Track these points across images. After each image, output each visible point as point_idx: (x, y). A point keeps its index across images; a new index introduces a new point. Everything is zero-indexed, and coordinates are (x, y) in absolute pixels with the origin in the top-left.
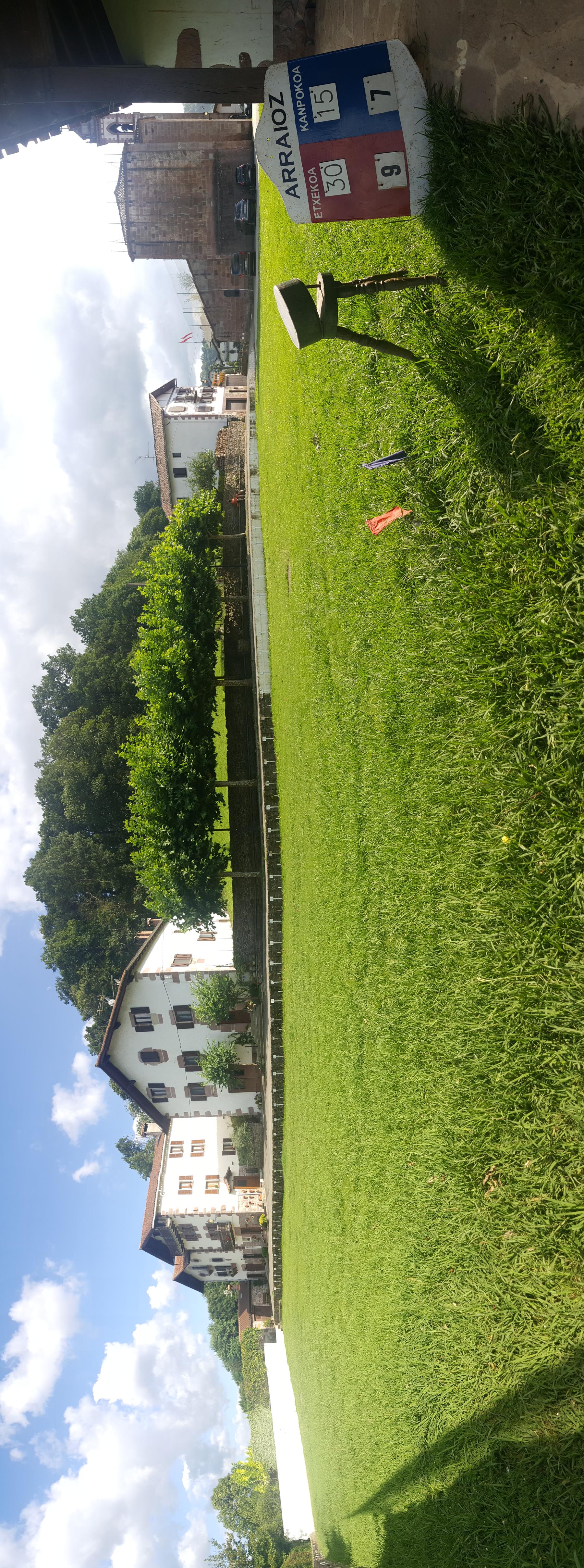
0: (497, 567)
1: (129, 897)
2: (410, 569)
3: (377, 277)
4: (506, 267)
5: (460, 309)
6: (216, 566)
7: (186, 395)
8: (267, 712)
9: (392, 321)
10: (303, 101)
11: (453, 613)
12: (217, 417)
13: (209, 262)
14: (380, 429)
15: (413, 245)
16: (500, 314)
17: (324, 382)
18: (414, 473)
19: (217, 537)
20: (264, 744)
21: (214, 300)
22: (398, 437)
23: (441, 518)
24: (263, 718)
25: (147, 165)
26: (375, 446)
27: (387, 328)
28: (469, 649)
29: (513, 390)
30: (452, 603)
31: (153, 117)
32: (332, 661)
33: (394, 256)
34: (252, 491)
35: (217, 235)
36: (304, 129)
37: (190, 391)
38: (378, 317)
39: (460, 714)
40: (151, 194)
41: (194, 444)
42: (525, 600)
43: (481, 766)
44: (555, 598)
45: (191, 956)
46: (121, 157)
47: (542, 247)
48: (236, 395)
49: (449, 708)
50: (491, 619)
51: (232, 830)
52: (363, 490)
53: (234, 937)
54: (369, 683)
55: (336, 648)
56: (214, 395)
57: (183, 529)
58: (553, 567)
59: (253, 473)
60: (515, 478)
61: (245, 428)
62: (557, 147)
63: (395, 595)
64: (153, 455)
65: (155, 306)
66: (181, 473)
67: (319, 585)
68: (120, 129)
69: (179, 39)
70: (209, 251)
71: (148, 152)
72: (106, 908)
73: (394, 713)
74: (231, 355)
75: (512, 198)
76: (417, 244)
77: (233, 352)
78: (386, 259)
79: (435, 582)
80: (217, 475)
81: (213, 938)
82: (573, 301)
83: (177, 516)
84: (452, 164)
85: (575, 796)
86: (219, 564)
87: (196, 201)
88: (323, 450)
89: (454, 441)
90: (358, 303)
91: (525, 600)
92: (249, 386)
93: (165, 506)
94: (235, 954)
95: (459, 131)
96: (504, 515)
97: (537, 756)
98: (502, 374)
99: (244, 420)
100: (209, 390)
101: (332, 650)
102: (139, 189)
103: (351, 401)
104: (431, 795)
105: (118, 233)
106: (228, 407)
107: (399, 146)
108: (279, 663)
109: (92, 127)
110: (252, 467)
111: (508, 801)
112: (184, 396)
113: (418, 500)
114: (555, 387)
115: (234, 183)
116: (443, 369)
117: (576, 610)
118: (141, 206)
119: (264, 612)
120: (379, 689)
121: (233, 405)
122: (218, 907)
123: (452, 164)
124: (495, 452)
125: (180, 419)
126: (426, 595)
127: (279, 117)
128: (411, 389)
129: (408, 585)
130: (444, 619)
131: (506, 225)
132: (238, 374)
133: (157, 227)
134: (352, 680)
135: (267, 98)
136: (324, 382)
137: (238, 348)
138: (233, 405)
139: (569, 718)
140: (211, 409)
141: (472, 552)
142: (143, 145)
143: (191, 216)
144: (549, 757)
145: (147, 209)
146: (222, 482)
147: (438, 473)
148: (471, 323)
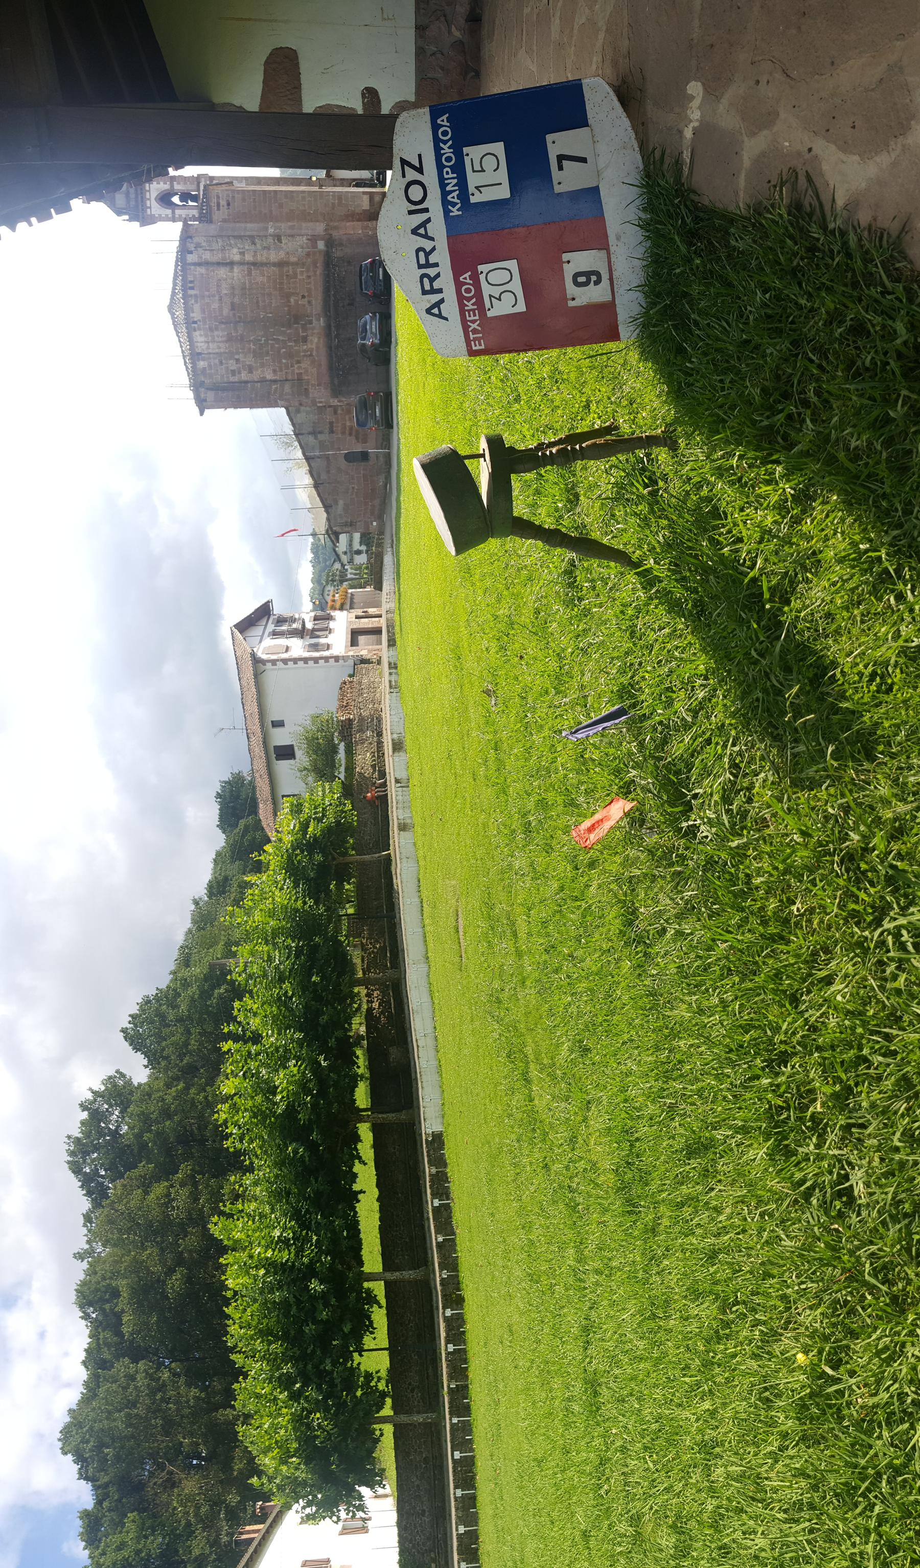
0: (773, 904)
1: (227, 1466)
2: (642, 910)
3: (573, 438)
4: (766, 423)
5: (699, 487)
6: (346, 915)
7: (287, 627)
8: (440, 1161)
9: (598, 505)
10: (453, 169)
11: (707, 990)
12: (337, 659)
13: (321, 410)
14: (588, 675)
15: (626, 387)
16: (759, 496)
17: (499, 601)
18: (641, 745)
19: (348, 859)
20: (436, 1210)
21: (328, 472)
22: (615, 689)
23: (684, 824)
24: (434, 1170)
25: (218, 257)
26: (581, 701)
27: (590, 517)
28: (731, 1051)
29: (783, 613)
30: (705, 970)
31: (229, 182)
32: (534, 1073)
33: (598, 403)
34: (397, 781)
35: (331, 368)
36: (455, 212)
37: (293, 620)
38: (577, 496)
39: (722, 1157)
40: (226, 312)
41: (303, 704)
42: (812, 960)
43: (761, 1230)
44: (857, 955)
45: (328, 1561)
46: (177, 244)
47: (818, 393)
48: (366, 623)
49: (706, 1148)
50: (761, 997)
51: (393, 1350)
52: (566, 776)
53: (399, 1524)
54: (588, 1109)
55: (537, 1055)
56: (332, 624)
57: (294, 850)
58: (857, 903)
59: (398, 746)
60: (794, 756)
61: (381, 675)
62: (832, 251)
63: (619, 960)
64: (240, 723)
65: (240, 482)
66: (286, 753)
67: (507, 945)
68: (176, 199)
69: (266, 63)
70: (321, 395)
71: (221, 236)
72: (190, 1485)
73: (628, 1156)
74: (356, 556)
75: (769, 317)
76: (632, 384)
77: (359, 552)
78: (587, 406)
79: (680, 934)
80: (341, 755)
81: (364, 1529)
82: (869, 476)
83: (282, 829)
84: (678, 271)
85: (903, 1275)
86: (351, 911)
87: (297, 318)
88: (501, 707)
89: (701, 695)
90: (547, 476)
91: (812, 960)
92: (385, 607)
93: (264, 811)
94: (401, 1553)
95: (688, 221)
96: (780, 813)
97: (841, 1215)
98: (765, 588)
99: (379, 662)
100: (323, 617)
101: (531, 1057)
102: (207, 300)
103: (540, 630)
104: (689, 1282)
105: (176, 373)
106: (354, 643)
107: (600, 242)
108: (454, 1089)
109: (132, 196)
110: (395, 736)
111: (803, 1286)
112: (284, 628)
113: (650, 792)
114: (847, 609)
115: (357, 295)
116: (676, 580)
117: (886, 980)
118: (211, 329)
119: (426, 998)
120: (604, 1122)
121: (362, 639)
122: (372, 1478)
123: (678, 271)
124: (763, 711)
125: (280, 665)
126: (668, 957)
127: (416, 193)
128: (630, 611)
129: (639, 940)
130: (694, 998)
131: (764, 356)
132: (368, 589)
133: (237, 360)
134: (563, 1105)
135: (397, 163)
136: (499, 601)
137: (367, 545)
138: (362, 639)
139: (882, 1160)
140: (328, 647)
141: (733, 880)
142: (213, 226)
143: (290, 340)
144: (859, 1214)
145: (220, 334)
146: (350, 769)
147: (678, 748)
148: (716, 508)
